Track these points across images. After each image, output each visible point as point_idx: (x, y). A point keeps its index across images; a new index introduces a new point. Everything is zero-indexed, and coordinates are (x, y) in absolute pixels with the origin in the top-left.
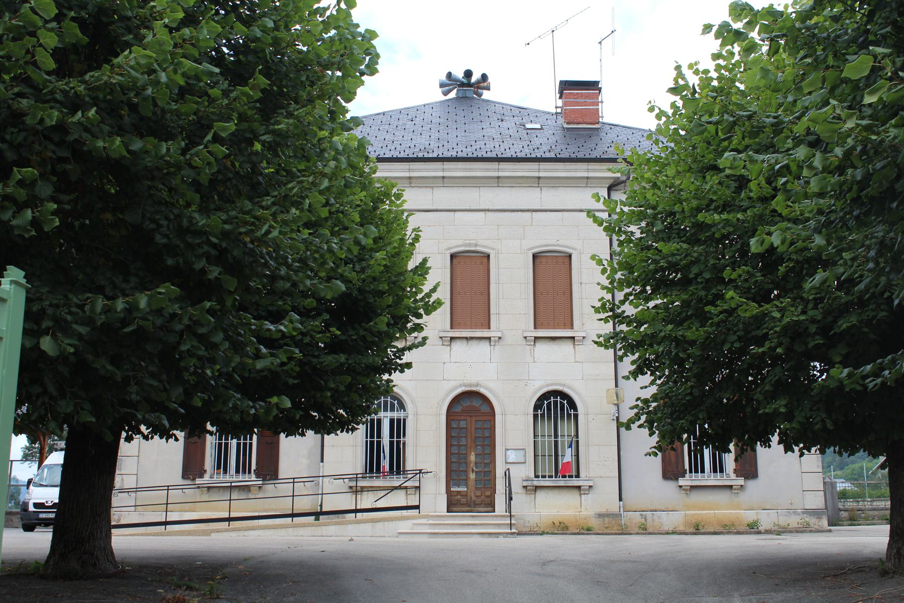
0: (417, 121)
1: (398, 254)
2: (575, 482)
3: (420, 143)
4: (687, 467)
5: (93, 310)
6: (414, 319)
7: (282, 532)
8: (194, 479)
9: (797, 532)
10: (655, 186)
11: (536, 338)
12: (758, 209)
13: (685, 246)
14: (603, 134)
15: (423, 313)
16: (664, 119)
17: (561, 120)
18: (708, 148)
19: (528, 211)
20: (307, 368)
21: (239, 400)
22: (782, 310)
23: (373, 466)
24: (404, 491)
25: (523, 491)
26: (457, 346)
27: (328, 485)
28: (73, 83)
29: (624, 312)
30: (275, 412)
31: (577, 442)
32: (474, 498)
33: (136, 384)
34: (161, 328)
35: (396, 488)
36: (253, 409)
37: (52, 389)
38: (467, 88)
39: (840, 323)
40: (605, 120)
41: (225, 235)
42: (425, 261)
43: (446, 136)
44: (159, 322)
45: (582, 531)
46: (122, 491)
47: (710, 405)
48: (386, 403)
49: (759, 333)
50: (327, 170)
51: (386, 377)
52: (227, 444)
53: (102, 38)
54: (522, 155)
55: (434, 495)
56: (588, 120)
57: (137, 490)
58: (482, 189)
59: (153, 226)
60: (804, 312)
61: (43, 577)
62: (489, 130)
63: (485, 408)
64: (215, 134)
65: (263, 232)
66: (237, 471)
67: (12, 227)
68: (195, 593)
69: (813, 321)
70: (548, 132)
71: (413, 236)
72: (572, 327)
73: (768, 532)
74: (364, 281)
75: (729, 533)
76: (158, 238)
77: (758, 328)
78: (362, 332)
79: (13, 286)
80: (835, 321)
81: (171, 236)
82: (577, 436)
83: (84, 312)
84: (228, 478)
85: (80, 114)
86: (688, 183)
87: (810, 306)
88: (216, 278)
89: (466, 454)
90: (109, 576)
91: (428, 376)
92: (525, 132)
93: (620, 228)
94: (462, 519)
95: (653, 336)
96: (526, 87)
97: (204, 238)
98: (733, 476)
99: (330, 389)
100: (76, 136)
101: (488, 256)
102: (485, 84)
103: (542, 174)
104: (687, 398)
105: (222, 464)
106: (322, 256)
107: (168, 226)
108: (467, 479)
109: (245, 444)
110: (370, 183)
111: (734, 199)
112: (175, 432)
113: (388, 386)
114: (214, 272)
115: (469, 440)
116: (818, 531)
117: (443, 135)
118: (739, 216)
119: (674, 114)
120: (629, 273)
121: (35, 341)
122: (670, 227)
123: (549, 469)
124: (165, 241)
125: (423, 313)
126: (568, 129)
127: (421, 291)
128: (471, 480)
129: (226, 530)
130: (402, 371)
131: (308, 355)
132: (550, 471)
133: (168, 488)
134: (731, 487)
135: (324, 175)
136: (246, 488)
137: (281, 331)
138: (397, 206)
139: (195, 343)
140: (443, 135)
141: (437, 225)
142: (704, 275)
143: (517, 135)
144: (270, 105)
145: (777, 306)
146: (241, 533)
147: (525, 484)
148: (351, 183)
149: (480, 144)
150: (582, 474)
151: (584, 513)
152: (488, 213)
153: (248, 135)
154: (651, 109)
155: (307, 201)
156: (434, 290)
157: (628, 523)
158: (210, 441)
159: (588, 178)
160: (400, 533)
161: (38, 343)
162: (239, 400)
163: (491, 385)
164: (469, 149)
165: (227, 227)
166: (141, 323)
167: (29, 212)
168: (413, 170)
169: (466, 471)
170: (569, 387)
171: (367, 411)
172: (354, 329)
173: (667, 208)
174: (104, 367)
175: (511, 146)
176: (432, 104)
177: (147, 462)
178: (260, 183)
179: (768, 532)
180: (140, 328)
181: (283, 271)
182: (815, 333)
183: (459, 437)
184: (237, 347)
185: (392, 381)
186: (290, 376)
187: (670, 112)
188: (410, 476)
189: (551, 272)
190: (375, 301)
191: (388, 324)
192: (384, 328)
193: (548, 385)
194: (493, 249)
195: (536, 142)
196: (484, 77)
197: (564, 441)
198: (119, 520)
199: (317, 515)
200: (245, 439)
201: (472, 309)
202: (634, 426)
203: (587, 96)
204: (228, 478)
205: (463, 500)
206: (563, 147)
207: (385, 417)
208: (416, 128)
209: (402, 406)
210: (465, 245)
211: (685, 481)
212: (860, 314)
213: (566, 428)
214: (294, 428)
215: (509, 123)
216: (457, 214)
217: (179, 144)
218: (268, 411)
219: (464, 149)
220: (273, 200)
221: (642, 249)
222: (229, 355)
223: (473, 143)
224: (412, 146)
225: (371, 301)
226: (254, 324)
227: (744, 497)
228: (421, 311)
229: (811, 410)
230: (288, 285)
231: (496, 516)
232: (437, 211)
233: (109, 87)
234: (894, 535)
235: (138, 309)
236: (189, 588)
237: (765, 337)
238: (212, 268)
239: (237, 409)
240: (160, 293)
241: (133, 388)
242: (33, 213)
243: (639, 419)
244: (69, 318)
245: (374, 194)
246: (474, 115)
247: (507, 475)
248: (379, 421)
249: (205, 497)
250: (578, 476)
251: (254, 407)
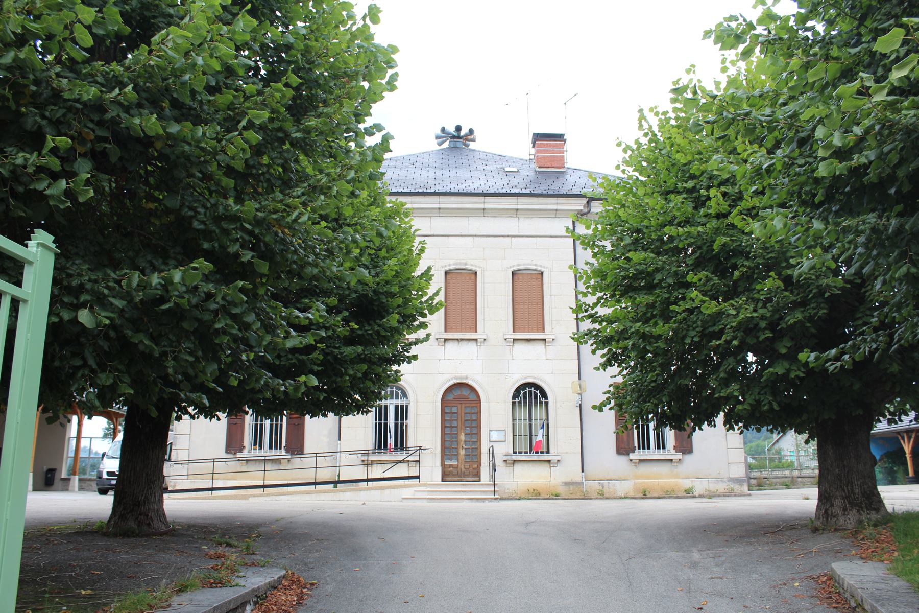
0: (417, 165)
1: (407, 262)
2: (545, 457)
4: (636, 444)
5: (129, 284)
7: (307, 497)
8: (235, 454)
10: (623, 206)
12: (714, 223)
13: (652, 255)
14: (567, 177)
16: (629, 152)
17: (534, 166)
21: (270, 378)
23: (381, 443)
25: (504, 464)
27: (344, 459)
28: (115, 66)
29: (597, 313)
30: (303, 389)
33: (174, 359)
34: (196, 306)
35: (400, 462)
36: (283, 386)
37: (91, 362)
38: (457, 140)
41: (258, 222)
42: (429, 269)
44: (194, 301)
46: (177, 462)
47: (667, 390)
48: (392, 392)
49: (716, 328)
50: (353, 163)
51: (395, 367)
52: (261, 425)
53: (143, 26)
54: (504, 191)
55: (431, 467)
57: (189, 462)
59: (191, 213)
60: (755, 311)
61: (106, 535)
63: (472, 397)
64: (249, 121)
66: (270, 447)
67: (47, 197)
68: (234, 550)
69: (762, 317)
71: (419, 247)
72: (543, 331)
73: (701, 496)
74: (378, 284)
75: (670, 497)
77: (714, 325)
78: (376, 328)
79: (40, 249)
82: (547, 419)
83: (121, 286)
85: (117, 91)
87: (760, 305)
90: (161, 534)
91: (426, 372)
93: (594, 242)
94: (454, 487)
95: (625, 331)
96: (505, 141)
97: (239, 224)
98: (673, 452)
100: (114, 114)
101: (476, 273)
103: (519, 207)
105: (258, 441)
106: (347, 246)
107: (205, 214)
109: (277, 425)
112: (218, 413)
114: (247, 256)
116: (741, 495)
118: (700, 229)
119: (638, 148)
121: (74, 314)
122: (636, 241)
123: (524, 445)
124: (202, 227)
126: (539, 172)
127: (426, 294)
128: (462, 455)
129: (261, 495)
130: (409, 362)
132: (525, 448)
133: (214, 460)
136: (278, 461)
137: (308, 318)
139: (229, 322)
141: (440, 245)
143: (499, 176)
144: (300, 107)
145: (733, 306)
146: (274, 498)
147: (505, 458)
149: (469, 183)
151: (553, 482)
153: (280, 135)
154: (619, 145)
155: (335, 188)
156: (436, 294)
158: (249, 420)
159: (556, 210)
161: (76, 316)
162: (270, 378)
164: (460, 186)
165: (260, 214)
166: (178, 301)
167: (64, 182)
168: (415, 203)
170: (542, 380)
171: (378, 396)
172: (370, 325)
174: (141, 342)
177: (195, 438)
179: (701, 496)
182: (765, 329)
183: (451, 421)
184: (270, 329)
186: (315, 364)
187: (635, 147)
189: (527, 286)
191: (399, 321)
192: (394, 324)
195: (514, 182)
196: (471, 131)
197: (537, 424)
198: (174, 486)
200: (277, 421)
203: (555, 146)
204: (263, 453)
205: (455, 472)
206: (537, 186)
207: (391, 404)
209: (405, 395)
210: (457, 264)
211: (635, 456)
212: (802, 312)
213: (538, 413)
214: (318, 410)
215: (491, 167)
218: (296, 389)
221: (613, 260)
225: (384, 301)
227: (681, 469)
228: (426, 311)
229: (759, 394)
230: (316, 271)
233: (149, 72)
234: (824, 498)
236: (229, 545)
237: (722, 332)
239: (268, 386)
242: (68, 183)
243: (610, 403)
244: (106, 291)
246: (463, 161)
248: (386, 407)
250: (548, 452)
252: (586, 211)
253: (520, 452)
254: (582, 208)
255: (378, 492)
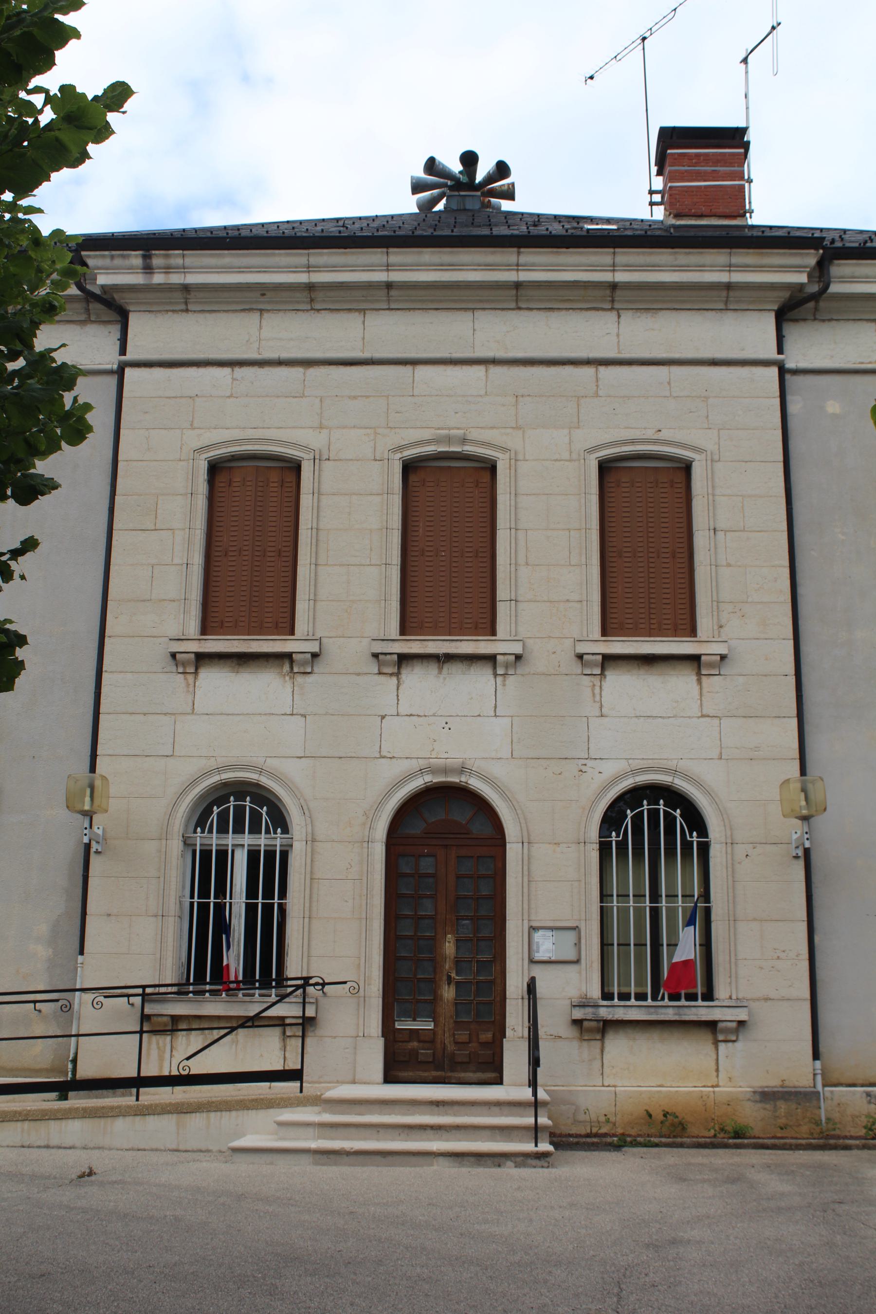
2: (701, 1011)
23: (204, 969)
25: (573, 1032)
26: (417, 679)
31: (708, 911)
45: (721, 1138)
48: (240, 812)
56: (721, 210)
58: (478, 313)
63: (481, 828)
72: (693, 631)
82: (706, 895)
89: (433, 938)
101: (492, 468)
103: (621, 277)
108: (436, 999)
123: (635, 974)
132: (640, 982)
147: (578, 1014)
150: (721, 991)
151: (725, 1089)
152: (495, 370)
157: (836, 1116)
163: (497, 770)
168: (317, 268)
188: (290, 990)
193: (635, 772)
194: (505, 450)
196: (502, 169)
205: (425, 1053)
209: (280, 821)
210: (437, 441)
213: (678, 878)
250: (709, 996)
252: (814, 288)
253: (625, 997)
254: (803, 278)
255: (168, 1122)
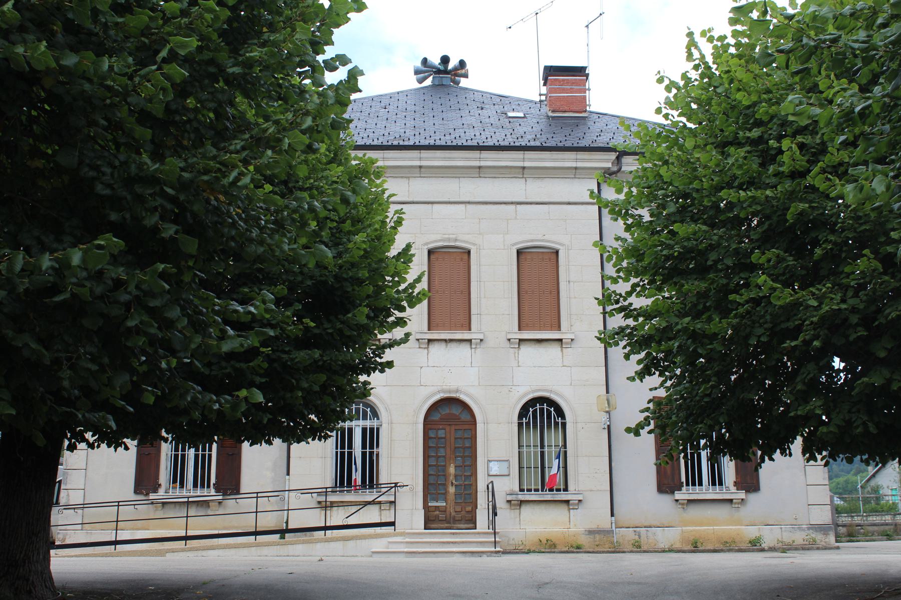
0: (391, 109)
1: (379, 238)
2: (563, 496)
3: (395, 132)
4: (683, 479)
6: (396, 312)
7: (245, 551)
8: (147, 494)
9: (803, 549)
10: (666, 163)
11: (521, 340)
12: (788, 185)
13: (704, 228)
14: (590, 123)
15: (406, 305)
16: (674, 91)
17: (545, 110)
18: (727, 120)
19: (512, 203)
20: (276, 365)
21: (200, 393)
22: (821, 299)
23: (343, 480)
24: (377, 506)
25: (507, 506)
26: (435, 349)
27: (294, 500)
29: (631, 304)
31: (565, 452)
32: (453, 514)
33: (70, 368)
34: (101, 297)
35: (369, 503)
38: (444, 75)
39: (887, 311)
40: (592, 109)
41: (183, 186)
42: (409, 246)
43: (422, 124)
44: (99, 290)
45: (571, 549)
46: (68, 507)
48: (358, 410)
51: (363, 378)
52: (183, 456)
54: (506, 143)
55: (411, 509)
56: (575, 108)
57: (84, 506)
59: (92, 174)
60: (843, 301)
62: (469, 118)
63: (465, 417)
64: (171, 51)
65: (231, 179)
66: (195, 485)
69: (854, 310)
70: (531, 121)
71: (395, 218)
72: (559, 328)
73: (772, 549)
74: (341, 267)
75: (730, 550)
76: (100, 189)
77: (788, 320)
78: (339, 325)
80: (879, 311)
81: (115, 186)
82: (565, 446)
84: (185, 493)
86: (709, 157)
87: (850, 293)
88: (171, 236)
89: (445, 466)
91: (404, 384)
92: (507, 120)
96: (508, 73)
97: (157, 189)
98: (733, 489)
99: (302, 390)
101: (469, 252)
102: (463, 71)
103: (527, 164)
104: (706, 400)
105: (178, 478)
107: (112, 175)
108: (446, 493)
109: (204, 456)
110: (346, 159)
111: (760, 174)
112: (125, 440)
113: (365, 389)
114: (170, 231)
115: (448, 449)
116: (826, 548)
117: (419, 123)
118: (768, 192)
119: (686, 85)
120: (637, 261)
122: (684, 208)
123: (534, 480)
124: (107, 192)
125: (406, 305)
127: (405, 280)
128: (451, 495)
129: (183, 550)
130: (382, 371)
131: (277, 351)
133: (118, 504)
134: (731, 501)
135: (307, 113)
136: (205, 504)
137: (250, 312)
138: (377, 186)
139: (145, 318)
140: (419, 123)
142: (725, 261)
143: (498, 123)
145: (813, 294)
146: (200, 553)
147: (509, 498)
148: (340, 123)
150: (571, 487)
152: (469, 206)
153: (212, 69)
154: (660, 80)
157: (621, 541)
158: (166, 449)
159: (576, 168)
160: (373, 552)
164: (448, 137)
165: (186, 175)
166: (77, 290)
169: (444, 485)
172: (329, 321)
173: (681, 188)
175: (493, 134)
176: (407, 91)
178: (227, 128)
179: (772, 549)
180: (74, 295)
181: (255, 233)
182: (857, 325)
183: (437, 448)
184: (199, 326)
185: (369, 383)
188: (384, 490)
189: (537, 268)
190: (353, 290)
191: (368, 317)
192: (364, 320)
193: (533, 391)
194: (474, 244)
195: (520, 131)
196: (462, 64)
197: (551, 452)
198: (64, 540)
199: (283, 532)
200: (204, 450)
201: (453, 312)
202: (644, 432)
205: (442, 516)
206: (549, 136)
207: (357, 426)
208: (389, 116)
209: (375, 414)
211: (682, 495)
213: (552, 438)
215: (489, 111)
216: (435, 206)
217: (125, 60)
218: (235, 407)
219: (443, 138)
220: (242, 143)
222: (188, 335)
223: (452, 131)
224: (386, 134)
225: (349, 289)
226: (219, 305)
227: (745, 512)
228: (405, 303)
229: (849, 412)
231: (479, 533)
232: (413, 203)
235: (69, 266)
237: (798, 329)
238: (166, 226)
240: (100, 247)
241: (66, 373)
243: (649, 424)
245: (351, 172)
246: (452, 103)
247: (491, 491)
248: (350, 430)
249: (160, 514)
250: (566, 489)
251: (218, 401)
